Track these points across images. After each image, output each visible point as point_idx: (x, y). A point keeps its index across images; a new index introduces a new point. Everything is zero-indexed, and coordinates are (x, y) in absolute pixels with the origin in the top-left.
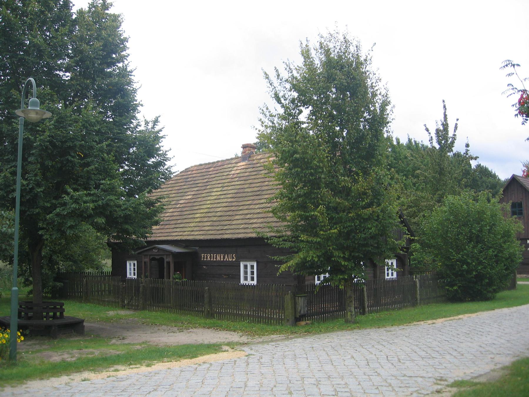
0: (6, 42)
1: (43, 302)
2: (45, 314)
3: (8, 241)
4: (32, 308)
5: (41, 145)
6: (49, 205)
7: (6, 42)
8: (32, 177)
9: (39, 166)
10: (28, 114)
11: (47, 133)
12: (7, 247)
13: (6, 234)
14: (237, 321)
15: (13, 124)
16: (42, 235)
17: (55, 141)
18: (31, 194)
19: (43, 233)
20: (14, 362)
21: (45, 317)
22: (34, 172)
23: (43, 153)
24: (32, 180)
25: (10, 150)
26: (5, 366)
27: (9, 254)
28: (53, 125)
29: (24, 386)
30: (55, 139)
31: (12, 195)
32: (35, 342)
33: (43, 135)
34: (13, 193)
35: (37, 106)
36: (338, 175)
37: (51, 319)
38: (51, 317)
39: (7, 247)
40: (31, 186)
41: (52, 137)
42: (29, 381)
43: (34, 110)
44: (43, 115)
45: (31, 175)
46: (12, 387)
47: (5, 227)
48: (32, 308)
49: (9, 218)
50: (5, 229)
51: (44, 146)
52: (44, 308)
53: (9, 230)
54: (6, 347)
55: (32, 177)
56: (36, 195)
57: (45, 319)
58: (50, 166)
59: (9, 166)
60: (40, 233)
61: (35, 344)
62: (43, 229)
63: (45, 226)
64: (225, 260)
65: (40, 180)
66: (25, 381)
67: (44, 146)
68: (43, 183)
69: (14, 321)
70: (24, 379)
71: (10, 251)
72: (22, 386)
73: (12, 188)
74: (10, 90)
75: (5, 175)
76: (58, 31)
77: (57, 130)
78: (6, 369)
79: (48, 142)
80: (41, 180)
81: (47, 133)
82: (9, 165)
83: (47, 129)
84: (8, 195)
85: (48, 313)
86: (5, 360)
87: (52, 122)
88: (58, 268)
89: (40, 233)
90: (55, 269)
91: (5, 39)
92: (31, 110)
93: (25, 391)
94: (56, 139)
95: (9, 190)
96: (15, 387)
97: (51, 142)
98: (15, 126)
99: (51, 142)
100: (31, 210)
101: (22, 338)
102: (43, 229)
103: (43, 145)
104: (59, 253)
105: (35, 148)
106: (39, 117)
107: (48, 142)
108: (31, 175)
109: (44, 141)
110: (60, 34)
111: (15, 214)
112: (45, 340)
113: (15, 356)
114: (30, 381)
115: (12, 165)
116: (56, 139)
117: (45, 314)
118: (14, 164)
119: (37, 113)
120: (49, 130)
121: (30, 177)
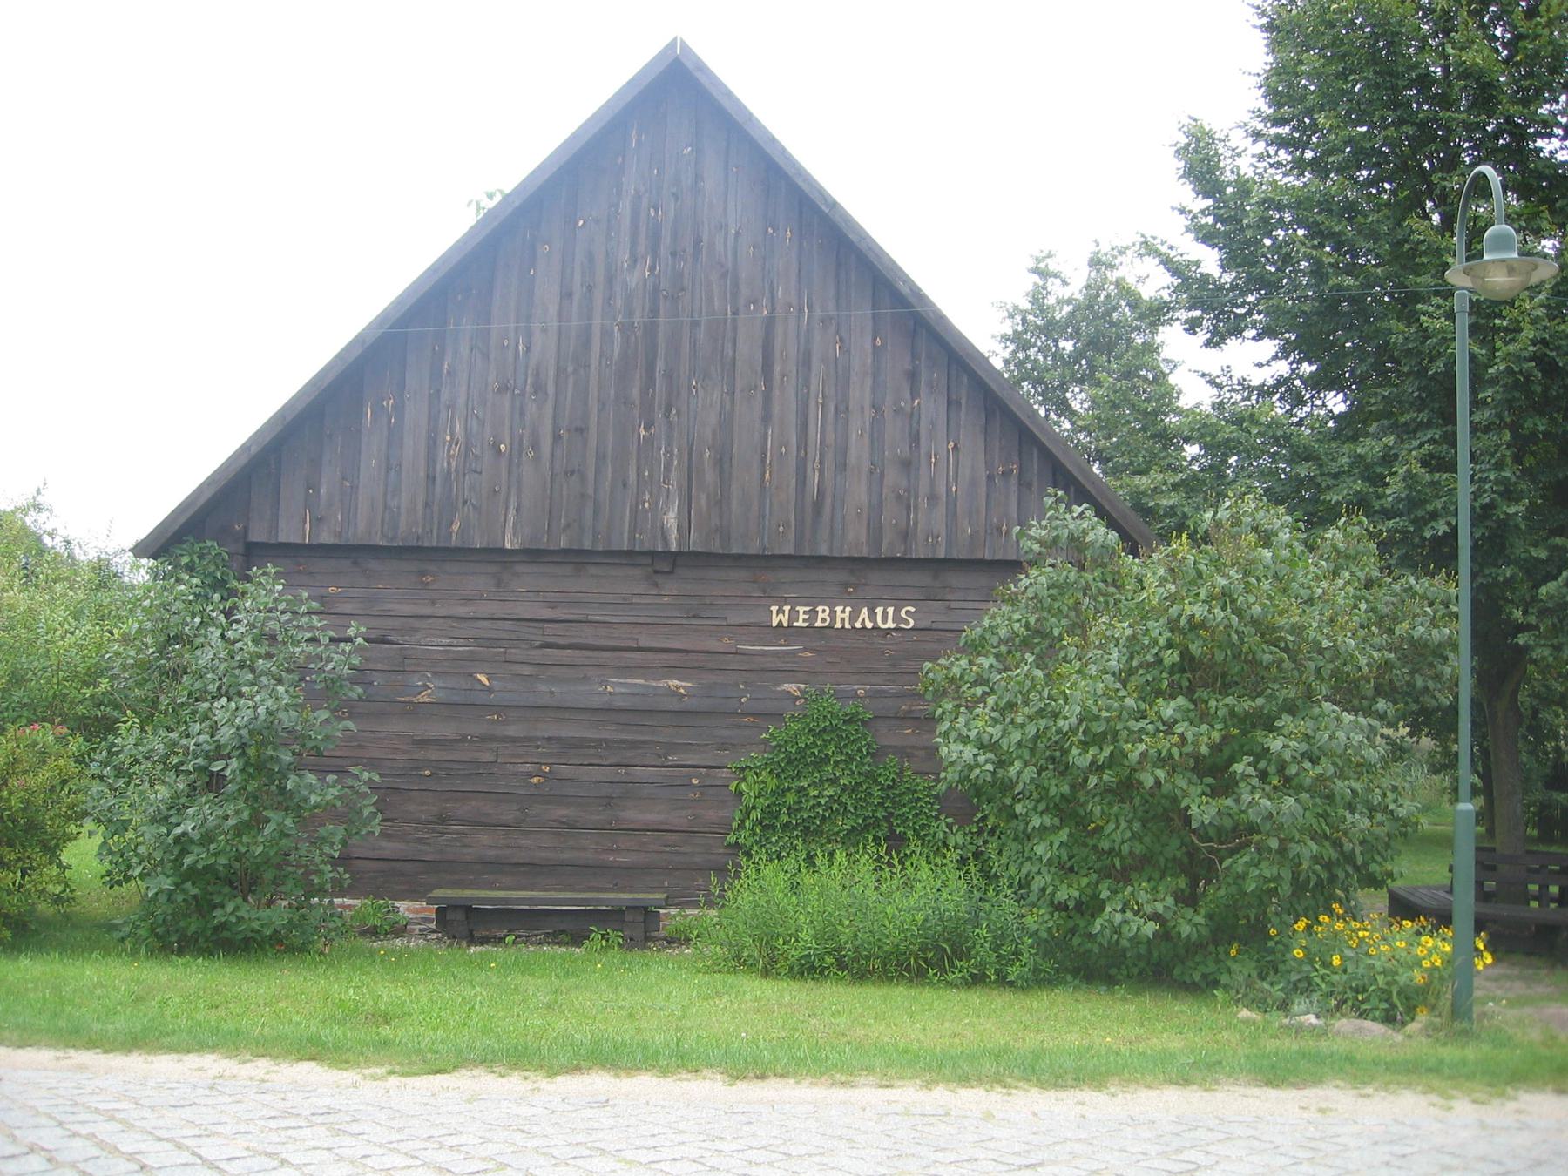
0: (1380, 80)
1: (1528, 852)
2: (1534, 888)
3: (1431, 665)
4: (1493, 868)
5: (1509, 371)
6: (1543, 555)
7: (1380, 80)
8: (1489, 470)
9: (1507, 436)
10: (1483, 279)
11: (1528, 333)
12: (1431, 684)
13: (1426, 645)
14: (55, 553)
15: (1422, 318)
16: (1526, 649)
17: (1554, 354)
18: (1488, 523)
19: (1531, 642)
20: (1465, 1025)
21: (1535, 898)
22: (1492, 455)
23: (1517, 395)
24: (1486, 480)
25: (1416, 394)
26: (1442, 1035)
27: (1434, 703)
28: (1542, 305)
29: (1511, 1105)
30: (1551, 350)
31: (1433, 528)
32: (1509, 972)
33: (1513, 340)
34: (1433, 524)
35: (1509, 248)
36: (1428, 478)
37: (1553, 906)
38: (1553, 900)
39: (1431, 684)
40: (1487, 500)
41: (1544, 342)
42: (1521, 1092)
43: (1503, 261)
44: (1529, 274)
45: (1483, 467)
46: (1475, 1102)
47: (1422, 625)
48: (1493, 868)
49: (1429, 595)
50: (1422, 629)
51: (1521, 372)
52: (1530, 871)
53: (1434, 632)
54: (1441, 979)
55: (1489, 470)
56: (1505, 524)
57: (1534, 904)
58: (1542, 433)
59: (1416, 443)
60: (1522, 640)
61: (1508, 977)
62: (1528, 628)
63: (1532, 620)
64: (858, 625)
65: (1513, 479)
66: (1509, 1090)
67: (1521, 372)
68: (1523, 486)
69: (1464, 905)
70: (1507, 1084)
71: (1438, 695)
72: (1502, 1105)
73: (1429, 508)
74: (1404, 219)
75: (1408, 471)
76: (1539, 14)
77: (1558, 320)
78: (1445, 1044)
79: (1530, 359)
80: (1518, 477)
81: (1528, 333)
82: (1415, 439)
83: (1527, 319)
84: (1420, 530)
85: (1544, 887)
86: (1440, 1015)
87: (1541, 297)
88: (1558, 749)
89: (1522, 640)
90: (1547, 753)
91: (1376, 72)
92: (1493, 261)
93: (1518, 1121)
94: (1558, 348)
95: (1420, 513)
96: (1483, 1103)
97: (1539, 359)
98: (1425, 325)
99: (1539, 359)
100: (1487, 572)
101: (1489, 960)
102: (1528, 628)
103: (1516, 369)
104: (1558, 704)
105: (1493, 381)
106: (1517, 279)
107: (1530, 359)
108: (1483, 467)
109: (1518, 358)
110: (1543, 21)
111: (1459, 590)
112: (1539, 968)
113: (1470, 1010)
114: (1526, 1091)
115: (1425, 439)
116: (1558, 348)
117: (1534, 888)
118: (1429, 436)
119: (1511, 270)
120: (1534, 322)
121: (1482, 471)
